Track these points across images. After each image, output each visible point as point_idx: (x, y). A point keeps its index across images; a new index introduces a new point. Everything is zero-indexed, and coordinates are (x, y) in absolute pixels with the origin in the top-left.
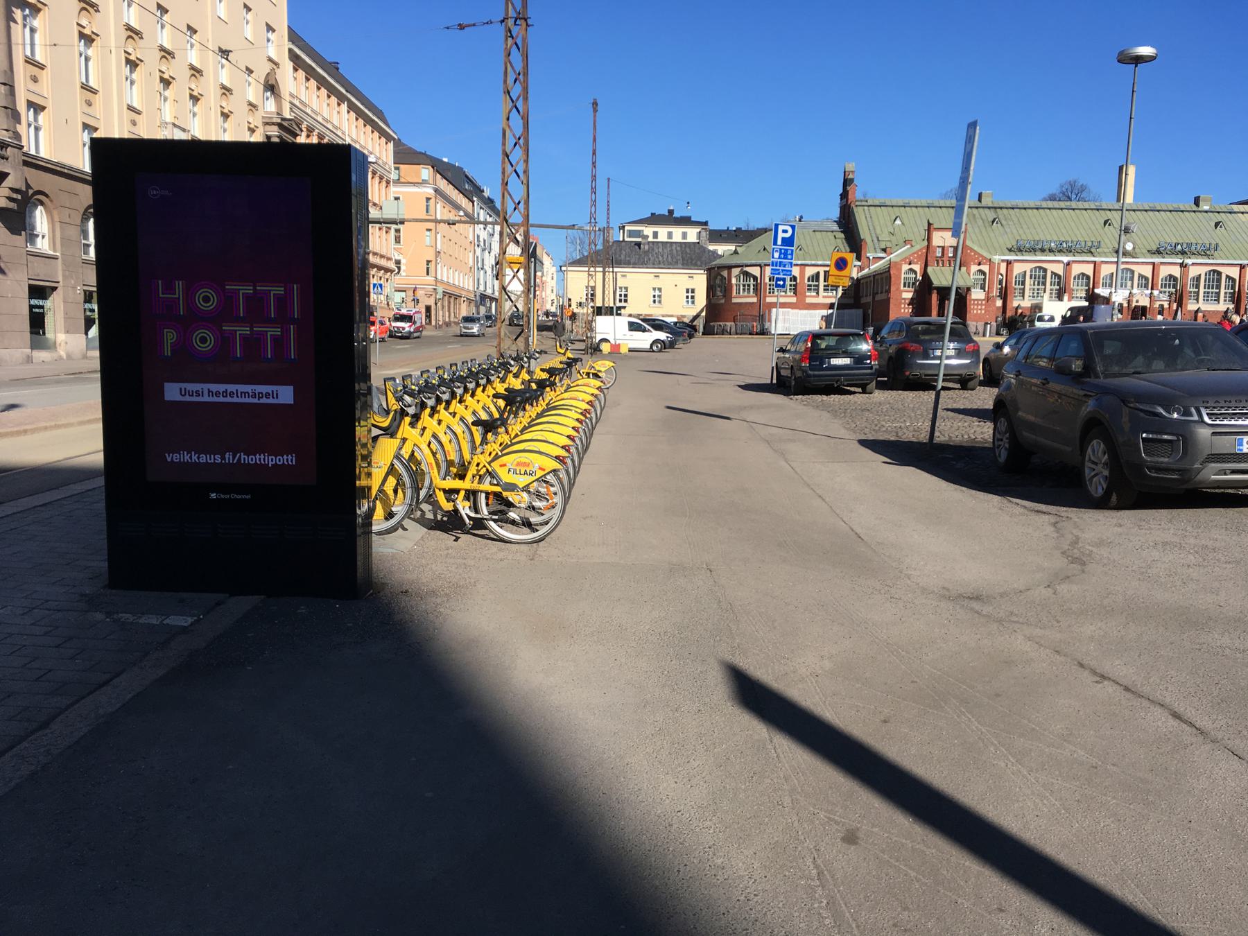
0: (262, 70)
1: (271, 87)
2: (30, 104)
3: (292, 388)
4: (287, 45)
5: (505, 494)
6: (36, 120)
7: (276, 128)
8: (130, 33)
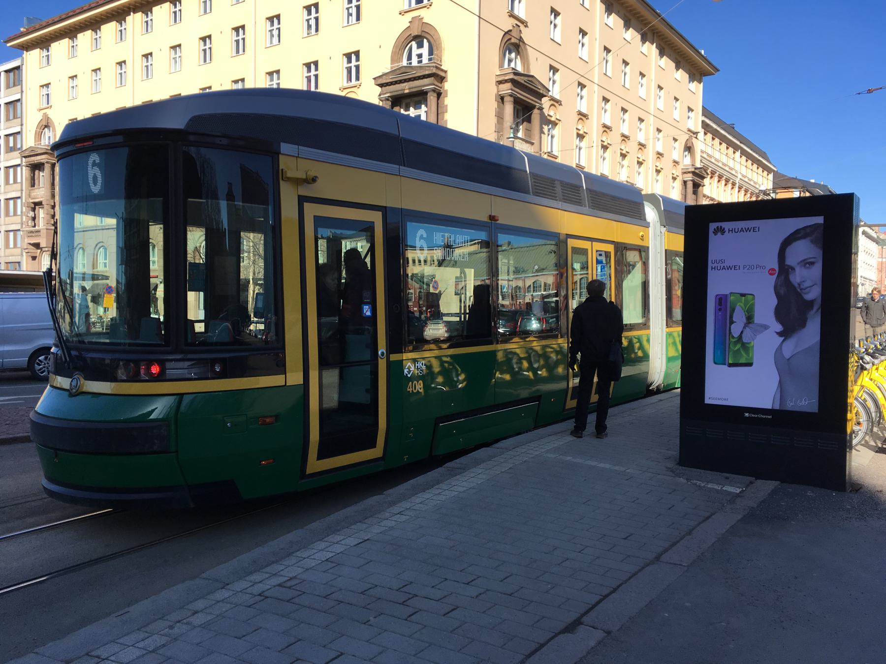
1: (689, 149)
4: (701, 118)
8: (552, 102)
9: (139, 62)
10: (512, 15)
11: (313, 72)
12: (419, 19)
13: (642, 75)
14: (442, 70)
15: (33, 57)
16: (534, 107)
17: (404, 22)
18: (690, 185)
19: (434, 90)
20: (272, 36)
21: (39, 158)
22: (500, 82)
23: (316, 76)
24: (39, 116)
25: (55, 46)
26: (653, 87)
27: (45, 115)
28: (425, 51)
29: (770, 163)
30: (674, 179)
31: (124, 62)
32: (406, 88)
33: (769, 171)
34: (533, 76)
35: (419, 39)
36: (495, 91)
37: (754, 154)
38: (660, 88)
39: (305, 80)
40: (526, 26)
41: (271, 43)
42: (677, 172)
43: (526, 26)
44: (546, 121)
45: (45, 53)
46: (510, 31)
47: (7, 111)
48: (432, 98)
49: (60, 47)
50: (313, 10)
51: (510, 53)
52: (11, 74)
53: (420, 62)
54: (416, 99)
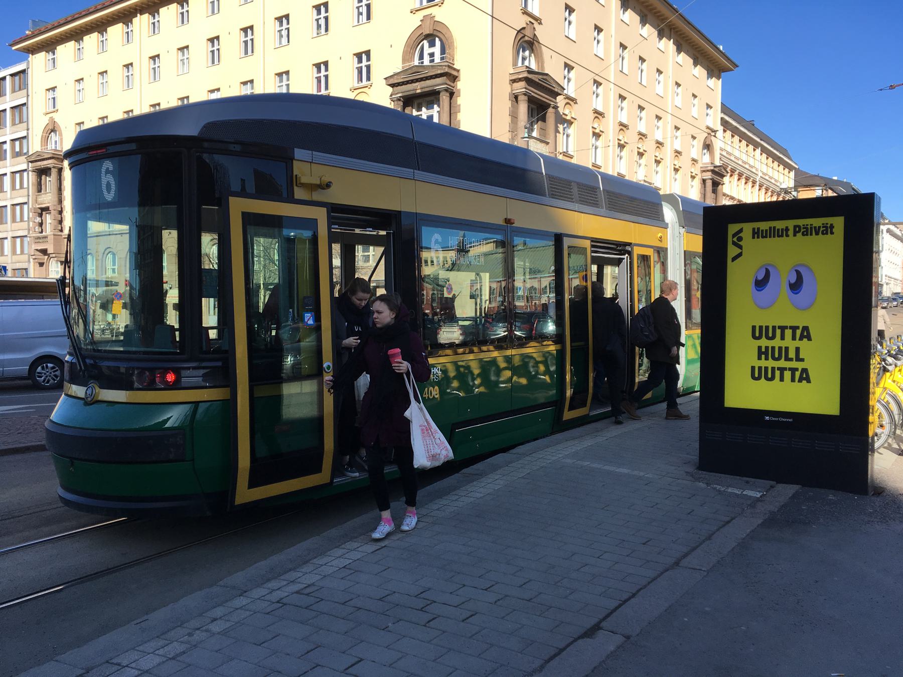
1: (708, 146)
4: (720, 115)
8: (567, 101)
10: (525, 12)
12: (431, 17)
13: (659, 72)
14: (455, 69)
15: (39, 60)
16: (548, 106)
17: (415, 21)
18: (709, 184)
19: (446, 90)
21: (45, 162)
22: (514, 81)
24: (45, 120)
25: (60, 49)
28: (437, 50)
30: (693, 177)
31: (131, 64)
32: (418, 88)
34: (547, 75)
35: (430, 38)
36: (509, 90)
40: (540, 23)
41: (280, 43)
42: (696, 170)
43: (540, 23)
45: (50, 56)
46: (524, 28)
47: (13, 116)
48: (444, 97)
49: (66, 50)
51: (524, 51)
52: (17, 78)
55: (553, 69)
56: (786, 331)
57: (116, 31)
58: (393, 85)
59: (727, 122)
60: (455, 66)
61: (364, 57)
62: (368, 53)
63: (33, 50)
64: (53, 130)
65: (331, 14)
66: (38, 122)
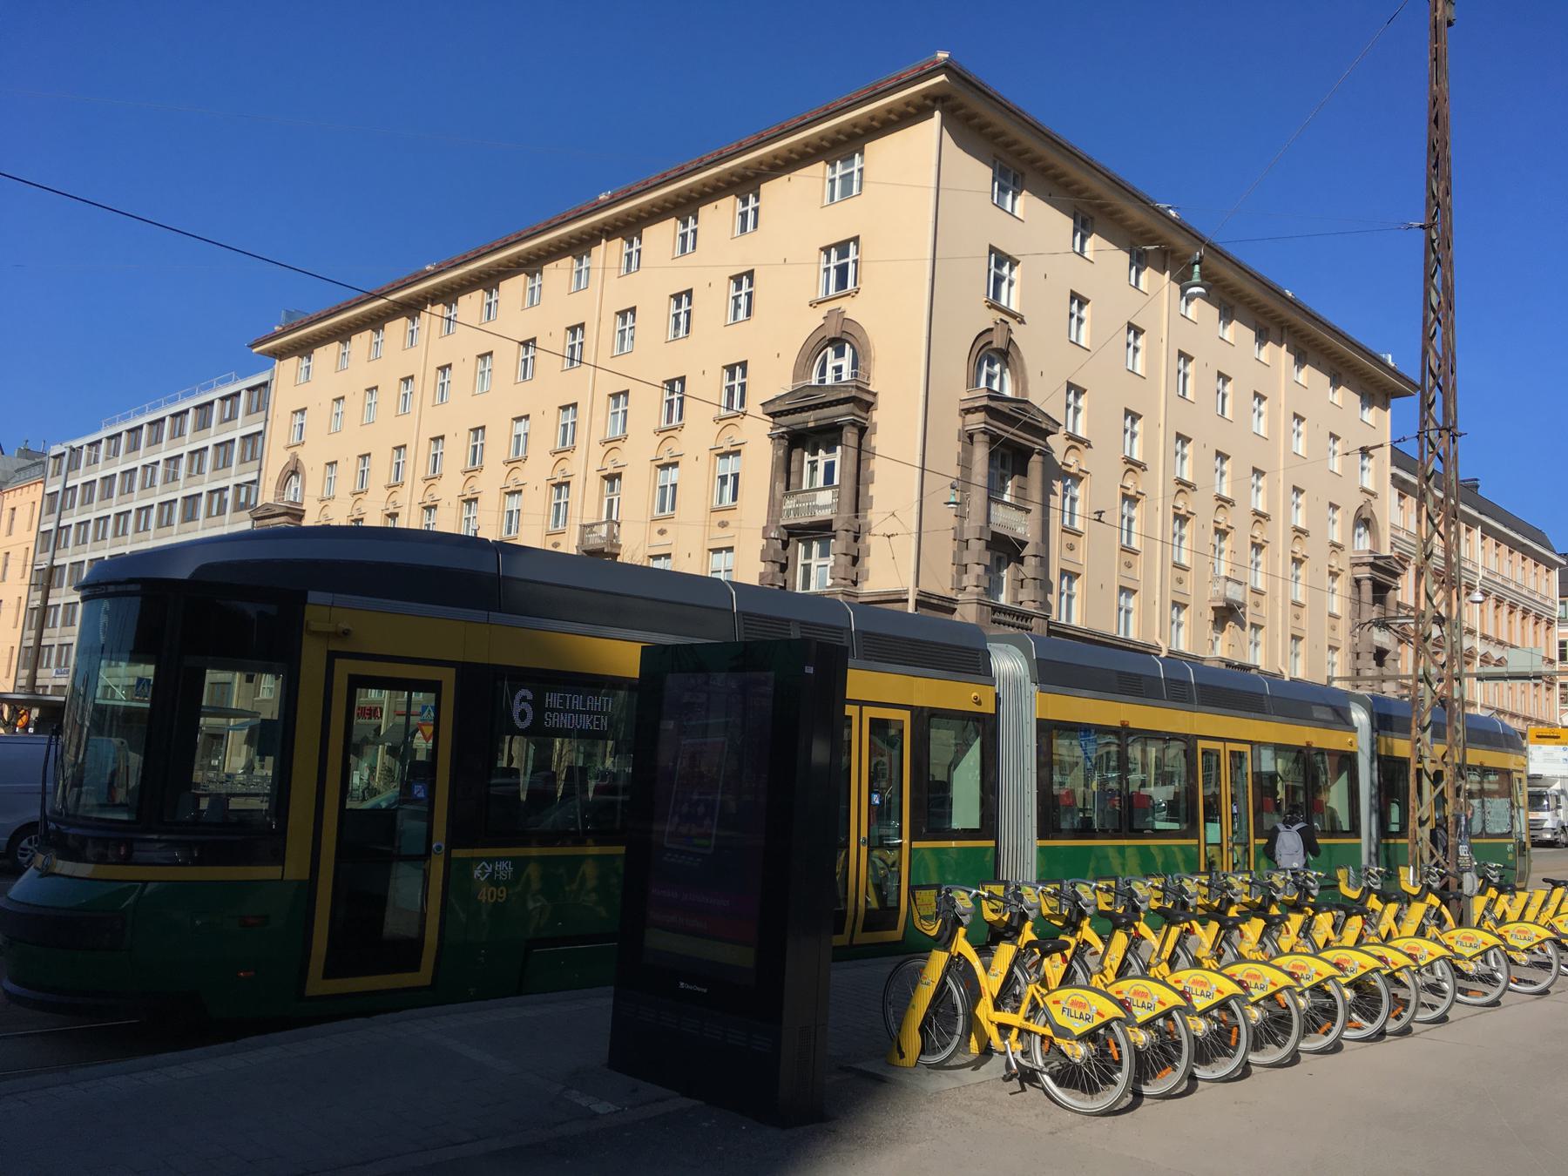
0: (1352, 502)
1: (1364, 521)
2: (1064, 573)
3: (275, 717)
4: (1389, 470)
5: (1057, 1040)
6: (1069, 587)
7: (981, 416)
8: (1072, 443)
9: (611, 324)
10: (994, 305)
11: (738, 379)
12: (839, 313)
13: (1260, 397)
14: (869, 392)
15: (289, 367)
16: (1031, 451)
17: (816, 318)
18: (1367, 587)
19: (853, 424)
20: (737, 306)
21: (276, 520)
22: (968, 411)
23: (743, 386)
24: (286, 457)
25: (319, 353)
26: (1284, 417)
27: (294, 455)
28: (846, 363)
29: (1553, 551)
30: (1334, 575)
31: (412, 377)
32: (810, 419)
33: (1550, 565)
34: (1027, 402)
35: (838, 344)
36: (960, 426)
37: (1512, 534)
38: (1299, 418)
39: (725, 393)
40: (1022, 322)
41: (622, 349)
42: (1341, 562)
43: (1022, 322)
44: (1054, 472)
45: (305, 363)
46: (990, 330)
47: (244, 449)
48: (850, 436)
49: (326, 355)
50: (745, 281)
51: (991, 364)
52: (256, 394)
53: (838, 378)
54: (830, 436)
55: (1045, 397)
56: (974, 822)
57: (397, 328)
58: (773, 415)
59: (1405, 482)
60: (870, 388)
61: (738, 371)
62: (744, 365)
63: (281, 354)
64: (295, 472)
65: (695, 308)
66: (275, 460)
